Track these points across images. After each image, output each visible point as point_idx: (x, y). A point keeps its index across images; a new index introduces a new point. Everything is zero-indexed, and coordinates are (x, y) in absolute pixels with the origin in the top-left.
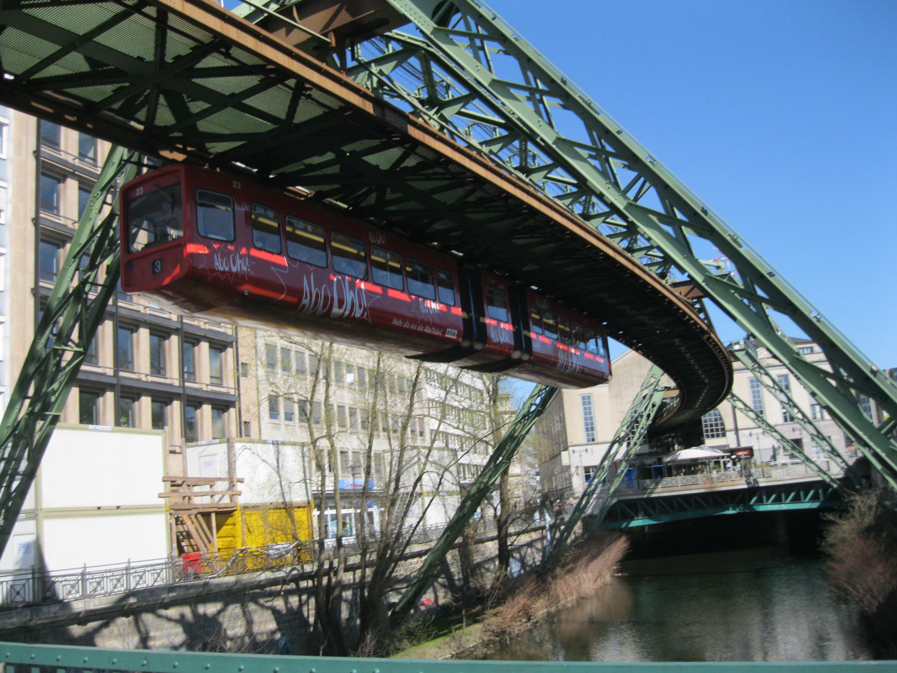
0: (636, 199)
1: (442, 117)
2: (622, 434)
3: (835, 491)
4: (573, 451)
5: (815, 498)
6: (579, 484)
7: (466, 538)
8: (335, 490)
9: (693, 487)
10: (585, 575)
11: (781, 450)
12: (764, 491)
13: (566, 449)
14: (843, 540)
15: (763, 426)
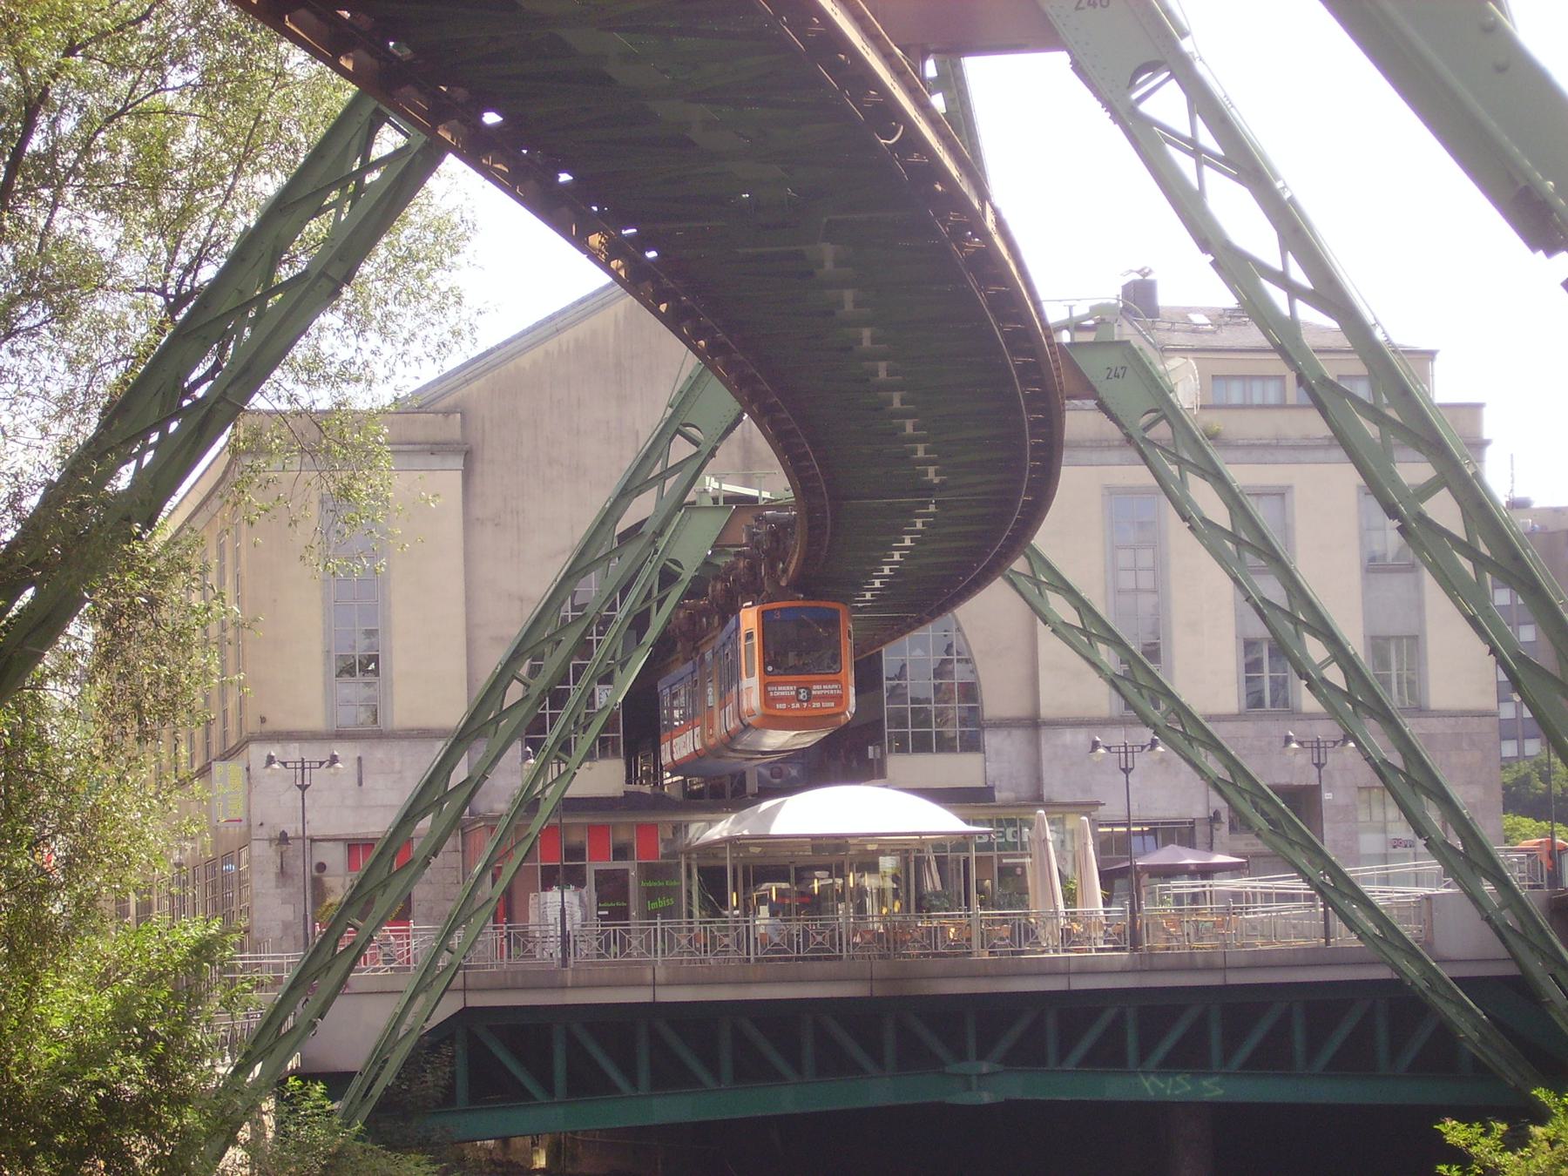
9: (818, 968)
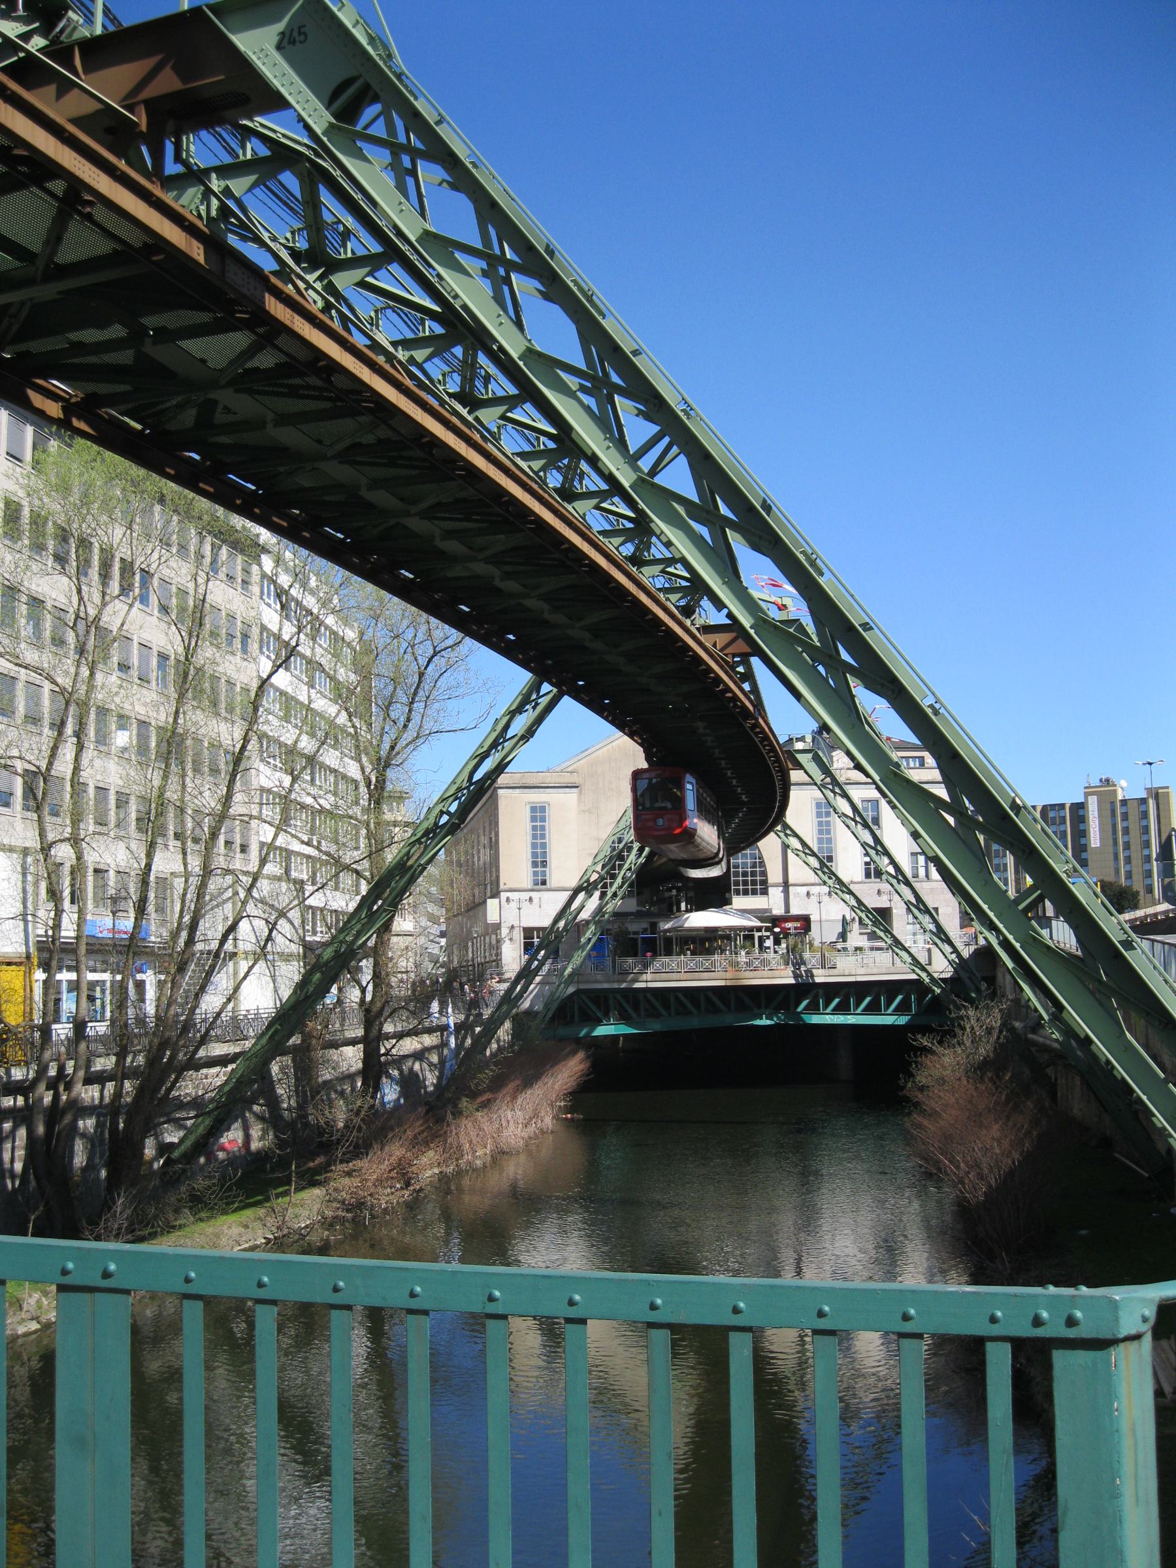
0: (654, 472)
1: (331, 289)
2: (595, 877)
3: (936, 998)
4: (508, 900)
5: (902, 1009)
6: (512, 957)
7: (307, 1037)
8: (78, 938)
10: (509, 1114)
11: (856, 925)
12: (821, 991)
13: (496, 894)
14: (942, 1081)
15: (830, 882)
